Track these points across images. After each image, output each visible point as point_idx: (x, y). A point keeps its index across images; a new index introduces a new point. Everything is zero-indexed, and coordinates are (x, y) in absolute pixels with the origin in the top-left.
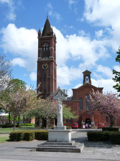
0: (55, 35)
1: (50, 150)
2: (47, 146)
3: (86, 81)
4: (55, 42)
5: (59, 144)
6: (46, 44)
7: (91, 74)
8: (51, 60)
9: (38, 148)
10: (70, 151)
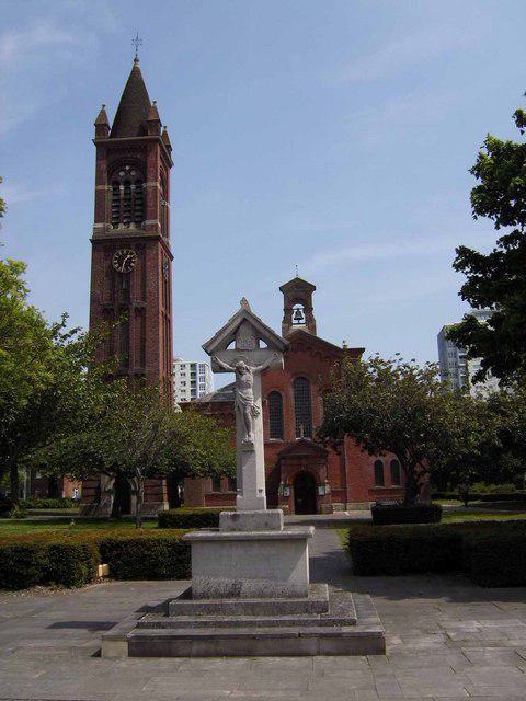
0: (165, 134)
1: (212, 648)
2: (185, 625)
3: (294, 322)
4: (168, 164)
5: (258, 609)
6: (127, 168)
7: (314, 295)
8: (150, 234)
9: (136, 637)
10: (326, 645)
